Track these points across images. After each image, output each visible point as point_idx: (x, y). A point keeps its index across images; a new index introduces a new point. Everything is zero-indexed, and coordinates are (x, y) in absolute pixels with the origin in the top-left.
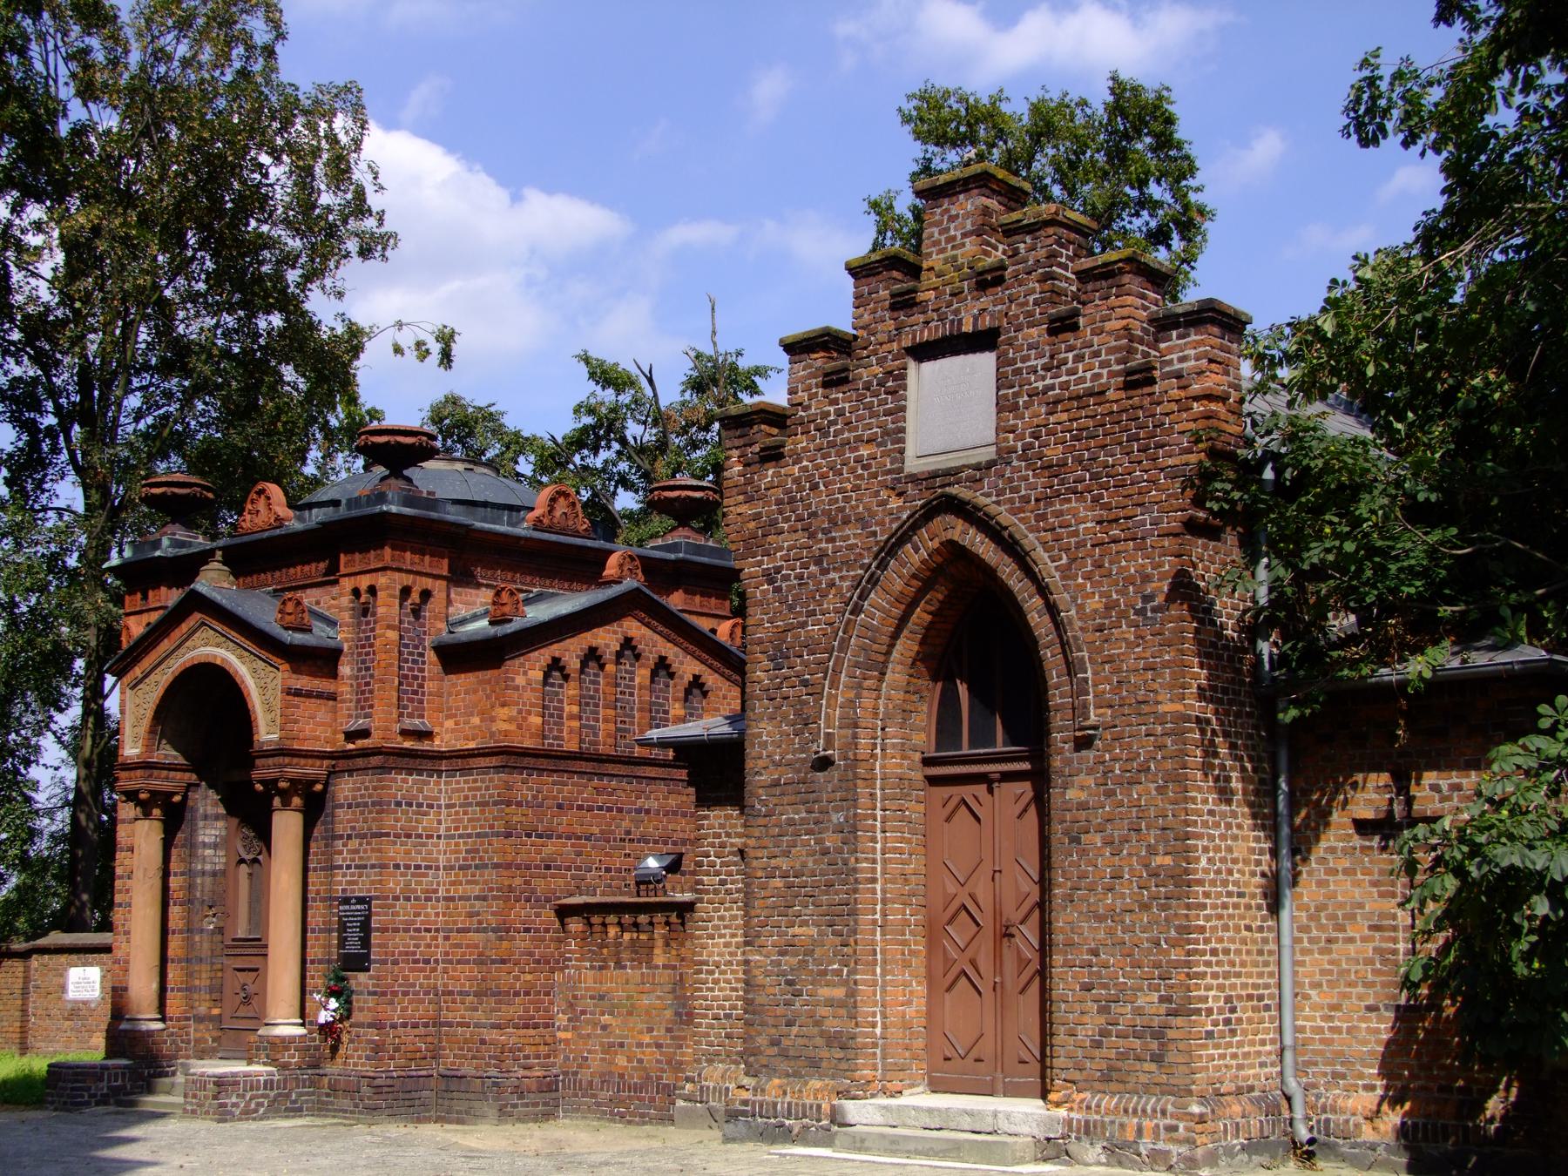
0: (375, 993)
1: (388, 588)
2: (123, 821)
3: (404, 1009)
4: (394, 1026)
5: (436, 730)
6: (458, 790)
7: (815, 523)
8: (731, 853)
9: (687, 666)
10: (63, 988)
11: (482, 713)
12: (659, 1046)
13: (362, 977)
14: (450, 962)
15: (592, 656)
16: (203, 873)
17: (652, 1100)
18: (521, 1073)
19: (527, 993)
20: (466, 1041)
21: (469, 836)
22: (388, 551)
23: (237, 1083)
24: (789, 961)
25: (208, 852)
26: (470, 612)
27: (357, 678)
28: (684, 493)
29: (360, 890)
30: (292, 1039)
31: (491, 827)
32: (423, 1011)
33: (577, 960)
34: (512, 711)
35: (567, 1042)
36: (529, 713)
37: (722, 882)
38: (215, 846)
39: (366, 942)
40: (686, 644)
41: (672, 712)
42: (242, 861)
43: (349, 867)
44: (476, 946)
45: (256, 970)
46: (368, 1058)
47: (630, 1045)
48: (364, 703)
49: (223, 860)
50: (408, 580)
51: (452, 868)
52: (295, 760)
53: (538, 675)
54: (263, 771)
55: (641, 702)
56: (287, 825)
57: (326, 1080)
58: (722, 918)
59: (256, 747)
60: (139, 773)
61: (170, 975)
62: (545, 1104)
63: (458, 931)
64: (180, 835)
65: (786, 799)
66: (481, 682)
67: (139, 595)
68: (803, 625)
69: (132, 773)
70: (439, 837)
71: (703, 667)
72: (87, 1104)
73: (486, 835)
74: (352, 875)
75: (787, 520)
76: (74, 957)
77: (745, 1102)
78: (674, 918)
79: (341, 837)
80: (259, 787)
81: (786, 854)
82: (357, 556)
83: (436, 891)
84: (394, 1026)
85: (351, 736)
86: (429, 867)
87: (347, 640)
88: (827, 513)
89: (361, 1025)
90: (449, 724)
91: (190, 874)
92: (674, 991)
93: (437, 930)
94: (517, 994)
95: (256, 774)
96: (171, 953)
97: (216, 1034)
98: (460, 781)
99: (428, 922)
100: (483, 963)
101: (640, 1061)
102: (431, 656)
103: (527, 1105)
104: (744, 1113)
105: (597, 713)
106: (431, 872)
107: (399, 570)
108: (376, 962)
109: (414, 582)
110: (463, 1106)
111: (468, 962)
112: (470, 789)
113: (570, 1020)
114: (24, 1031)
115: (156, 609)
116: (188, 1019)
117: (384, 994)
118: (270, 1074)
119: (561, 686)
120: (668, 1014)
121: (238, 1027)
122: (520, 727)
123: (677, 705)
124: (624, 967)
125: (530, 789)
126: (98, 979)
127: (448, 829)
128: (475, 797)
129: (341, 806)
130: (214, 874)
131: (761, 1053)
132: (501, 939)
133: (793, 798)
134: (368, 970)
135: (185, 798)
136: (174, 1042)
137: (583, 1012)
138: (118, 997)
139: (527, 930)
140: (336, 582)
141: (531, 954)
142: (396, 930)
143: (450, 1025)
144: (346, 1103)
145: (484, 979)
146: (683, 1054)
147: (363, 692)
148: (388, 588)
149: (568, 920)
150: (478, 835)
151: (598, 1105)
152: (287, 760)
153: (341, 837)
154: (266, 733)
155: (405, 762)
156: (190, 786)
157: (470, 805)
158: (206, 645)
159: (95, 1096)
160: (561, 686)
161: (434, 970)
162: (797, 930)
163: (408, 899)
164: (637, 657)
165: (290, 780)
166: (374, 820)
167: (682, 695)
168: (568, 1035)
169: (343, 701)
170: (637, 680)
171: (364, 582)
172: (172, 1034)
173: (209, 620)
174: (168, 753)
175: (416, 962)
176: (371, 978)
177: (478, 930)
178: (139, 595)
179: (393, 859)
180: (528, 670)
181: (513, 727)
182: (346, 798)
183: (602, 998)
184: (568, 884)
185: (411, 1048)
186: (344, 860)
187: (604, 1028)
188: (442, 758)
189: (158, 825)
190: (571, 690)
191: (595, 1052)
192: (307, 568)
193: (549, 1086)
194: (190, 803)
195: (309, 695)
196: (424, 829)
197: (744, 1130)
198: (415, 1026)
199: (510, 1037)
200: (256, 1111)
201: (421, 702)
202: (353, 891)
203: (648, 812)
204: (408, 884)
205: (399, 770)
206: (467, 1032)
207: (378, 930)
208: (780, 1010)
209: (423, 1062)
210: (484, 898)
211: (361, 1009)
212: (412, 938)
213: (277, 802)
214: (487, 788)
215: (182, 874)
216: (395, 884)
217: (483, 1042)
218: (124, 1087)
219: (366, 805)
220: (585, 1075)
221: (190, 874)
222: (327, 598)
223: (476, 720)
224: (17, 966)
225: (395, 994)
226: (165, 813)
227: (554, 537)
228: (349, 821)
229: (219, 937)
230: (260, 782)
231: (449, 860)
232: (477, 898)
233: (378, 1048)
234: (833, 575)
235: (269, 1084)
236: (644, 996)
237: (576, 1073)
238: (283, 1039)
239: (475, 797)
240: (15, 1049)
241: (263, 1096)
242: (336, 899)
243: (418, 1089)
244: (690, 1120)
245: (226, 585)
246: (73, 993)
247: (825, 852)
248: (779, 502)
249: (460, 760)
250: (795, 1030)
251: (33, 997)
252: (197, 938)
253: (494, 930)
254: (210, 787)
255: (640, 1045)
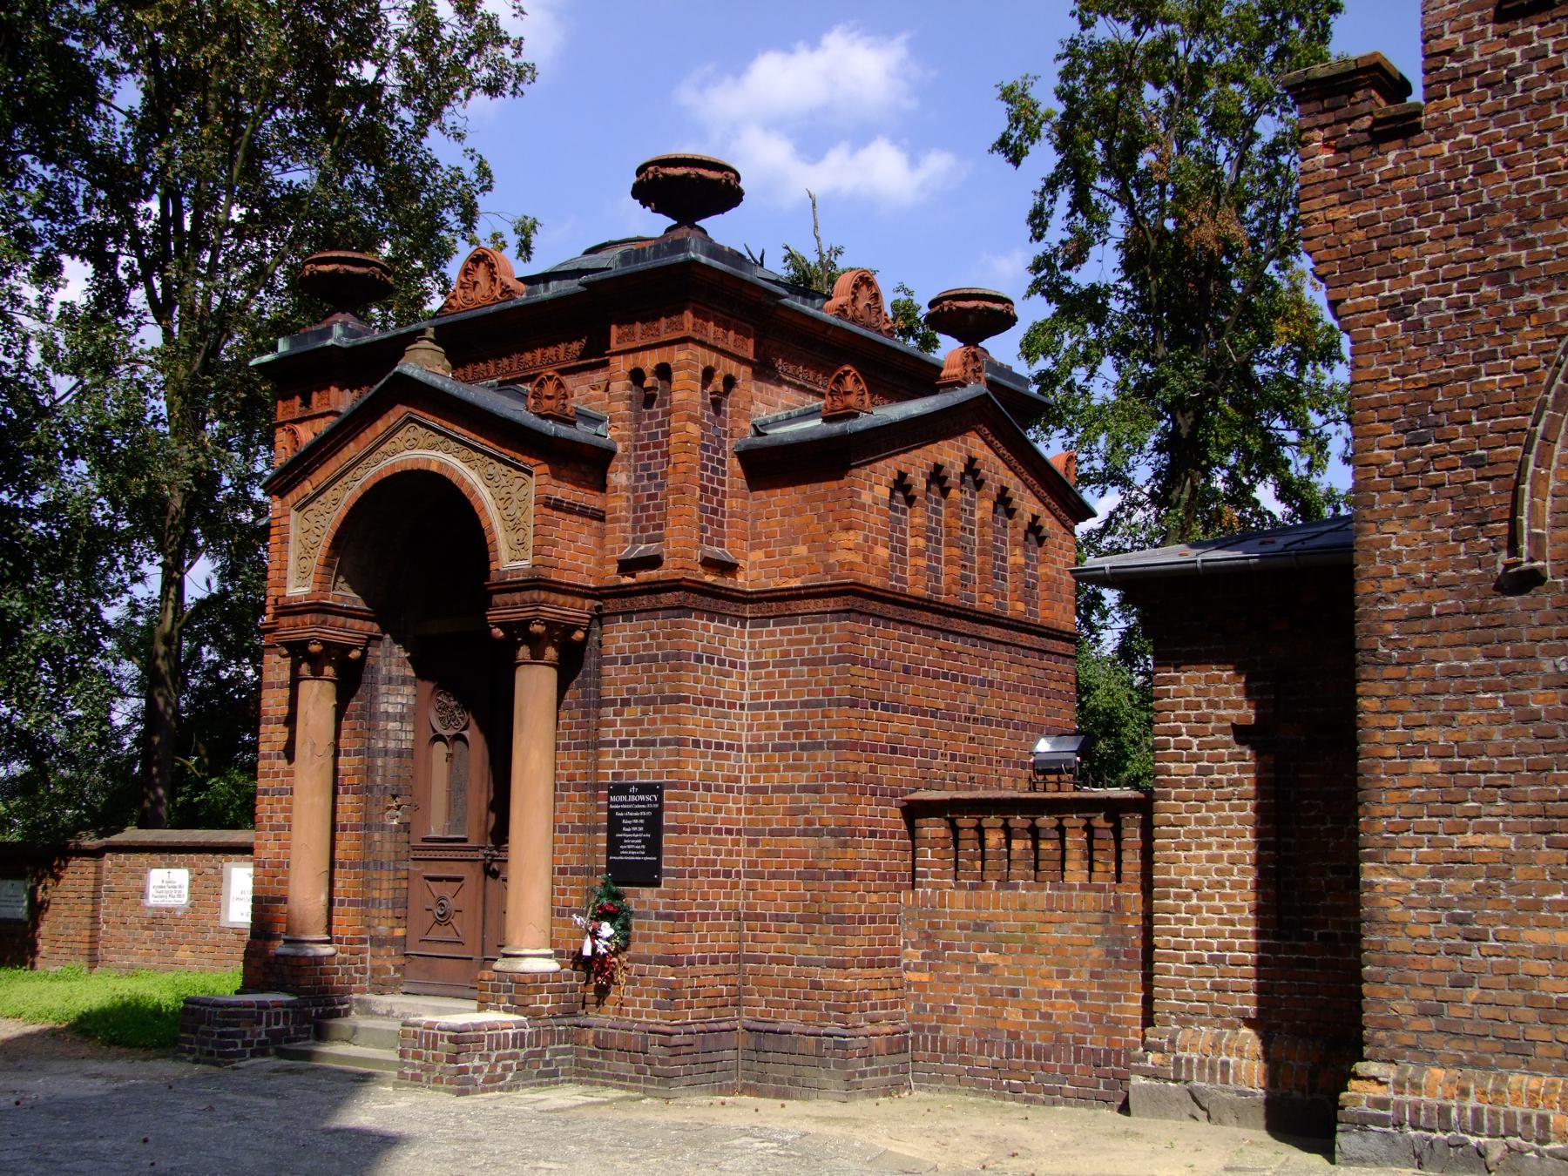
0: (668, 917)
1: (689, 366)
2: (272, 686)
3: (703, 939)
4: (691, 962)
5: (741, 563)
6: (771, 644)
7: (1490, 222)
8: (1223, 731)
9: (1028, 505)
10: (143, 893)
11: (811, 541)
12: (1077, 996)
13: (647, 893)
14: (760, 875)
15: (937, 476)
16: (386, 752)
17: (1067, 1070)
18: (870, 1028)
19: (873, 920)
20: (787, 983)
21: (791, 705)
22: (688, 317)
23: (480, 1039)
24: (1451, 887)
25: (392, 725)
26: (783, 411)
27: (635, 490)
28: (982, 304)
29: (643, 775)
30: (544, 977)
31: (831, 692)
32: (721, 941)
33: (934, 875)
34: (855, 537)
35: (920, 986)
36: (875, 542)
37: (1209, 771)
38: (401, 718)
39: (654, 846)
40: (1025, 476)
41: (1011, 560)
42: (438, 738)
43: (624, 743)
44: (803, 855)
45: (459, 880)
46: (658, 1006)
47: (1027, 995)
48: (648, 516)
49: (411, 736)
50: (712, 359)
51: (762, 748)
52: (553, 596)
53: (883, 492)
54: (503, 611)
55: (983, 542)
56: (535, 686)
57: (591, 1033)
58: (1203, 821)
59: (494, 578)
60: (308, 618)
61: (339, 885)
62: (895, 1070)
63: (772, 833)
64: (354, 702)
65: (1441, 639)
66: (808, 500)
67: (298, 400)
68: (1471, 375)
69: (299, 619)
70: (742, 707)
71: (1042, 508)
72: (241, 1055)
73: (819, 704)
74: (632, 754)
75: (1430, 222)
76: (157, 857)
77: (1383, 1104)
78: (1099, 820)
79: (613, 703)
80: (498, 633)
81: (1446, 721)
82: (638, 327)
83: (738, 780)
84: (691, 962)
85: (627, 566)
86: (730, 747)
87: (621, 439)
88: (1519, 207)
89: (646, 960)
90: (758, 556)
91: (368, 752)
92: (1104, 921)
93: (739, 832)
94: (862, 921)
95: (493, 616)
96: (339, 855)
97: (400, 961)
98: (774, 632)
99: (730, 821)
100: (813, 877)
101: (1046, 1016)
102: (734, 465)
103: (875, 1073)
104: (1381, 1121)
105: (939, 552)
106: (733, 753)
107: (702, 344)
108: (669, 873)
109: (718, 363)
110: (786, 1072)
111: (790, 876)
112: (791, 642)
113: (924, 956)
114: (94, 940)
115: (323, 415)
116: (363, 941)
117: (680, 918)
118: (520, 1025)
119: (904, 512)
120: (1096, 952)
121: (471, 963)
122: (866, 560)
123: (1018, 551)
124: (1015, 887)
125: (876, 644)
126: (186, 883)
127: (754, 696)
128: (799, 653)
129: (613, 661)
130: (400, 754)
131: (1401, 1026)
132: (844, 845)
133: (1457, 637)
134: (659, 885)
135: (365, 653)
136: (347, 971)
137: (947, 947)
138: (265, 906)
139: (873, 834)
140: (605, 364)
141: (877, 867)
142: (695, 831)
143: (759, 960)
144: (624, 1066)
145: (815, 900)
146: (1121, 1009)
147: (645, 508)
148: (689, 366)
149: (918, 822)
150: (805, 704)
151: (974, 1073)
152: (543, 595)
153: (613, 703)
154: (510, 557)
155: (707, 602)
156: (371, 640)
157: (793, 663)
158: (413, 447)
159: (250, 1043)
160: (904, 512)
161: (735, 886)
162: (1469, 838)
163: (708, 788)
164: (979, 484)
165: (547, 623)
166: (667, 679)
167: (1021, 538)
168: (925, 977)
169: (618, 520)
170: (978, 515)
171: (650, 361)
172: (344, 961)
173: (419, 414)
174: (344, 594)
175: (716, 874)
176: (661, 895)
177: (805, 833)
178: (298, 400)
179: (692, 732)
180: (872, 484)
181: (858, 559)
182: (620, 650)
183: (980, 927)
184: (913, 774)
185: (712, 992)
186: (616, 733)
187: (984, 968)
188: (746, 601)
189: (330, 687)
190: (917, 517)
191: (970, 1001)
192: (551, 351)
193: (897, 1045)
194: (370, 661)
195: (570, 509)
196: (727, 694)
197: (1383, 1148)
198: (714, 962)
199: (855, 979)
200: (502, 1077)
201: (721, 525)
202: (634, 776)
203: (991, 684)
204: (708, 768)
205: (701, 612)
206: (790, 972)
207: (673, 829)
208: (1440, 961)
209: (724, 1011)
210: (817, 790)
211: (645, 938)
212: (712, 842)
213: (524, 652)
214: (821, 641)
215: (357, 753)
216: (694, 767)
217: (816, 986)
218: (286, 1031)
219: (654, 659)
220: (951, 1032)
221: (368, 752)
222: (585, 388)
223: (802, 550)
224: (88, 866)
225: (692, 917)
226: (338, 672)
227: (863, 332)
228: (624, 681)
229: (405, 836)
230: (498, 625)
231: (756, 738)
232: (804, 789)
233: (672, 993)
234: (1528, 297)
235: (519, 1040)
236: (1052, 928)
237: (937, 1029)
238: (534, 976)
239: (799, 653)
240: (83, 962)
241: (513, 1056)
242: (602, 786)
243: (766, 1057)
244: (1160, 1106)
245: (440, 371)
246: (154, 899)
247: (1533, 718)
248: (1407, 198)
249: (774, 604)
250: (1473, 993)
251: (105, 902)
252: (377, 836)
253: (832, 833)
254: (396, 641)
255: (1045, 994)
